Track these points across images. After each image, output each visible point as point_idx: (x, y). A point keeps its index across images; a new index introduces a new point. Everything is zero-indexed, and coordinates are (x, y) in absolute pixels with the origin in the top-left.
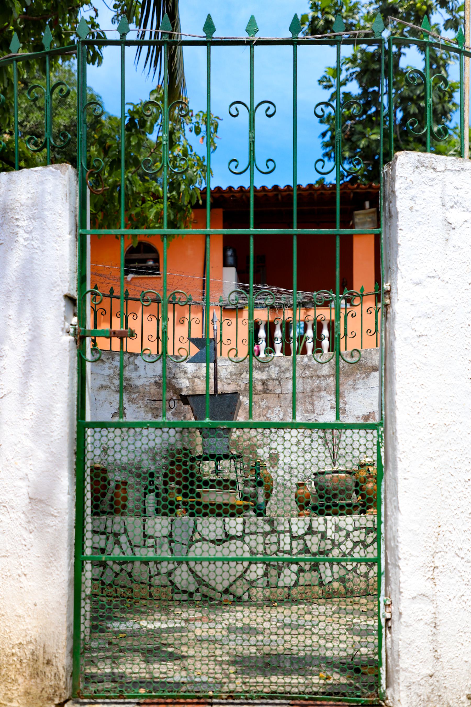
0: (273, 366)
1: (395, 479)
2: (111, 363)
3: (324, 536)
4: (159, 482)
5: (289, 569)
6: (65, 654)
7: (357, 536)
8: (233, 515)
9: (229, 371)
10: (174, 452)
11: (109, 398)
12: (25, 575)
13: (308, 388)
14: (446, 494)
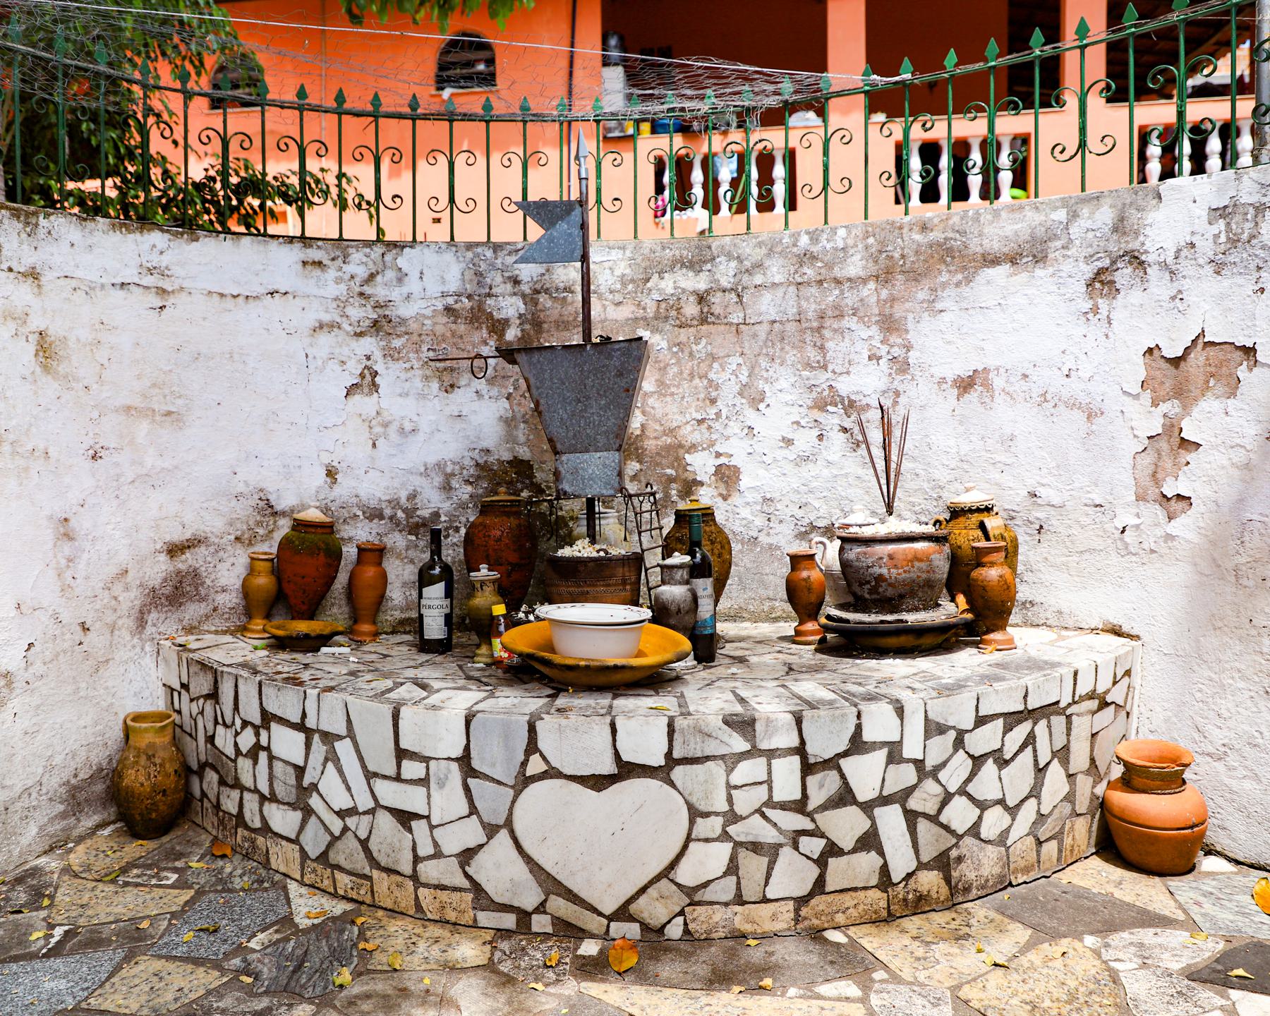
0: (722, 259)
2: (340, 269)
3: (894, 754)
4: (452, 552)
5: (796, 848)
9: (618, 272)
11: (337, 351)
13: (811, 309)
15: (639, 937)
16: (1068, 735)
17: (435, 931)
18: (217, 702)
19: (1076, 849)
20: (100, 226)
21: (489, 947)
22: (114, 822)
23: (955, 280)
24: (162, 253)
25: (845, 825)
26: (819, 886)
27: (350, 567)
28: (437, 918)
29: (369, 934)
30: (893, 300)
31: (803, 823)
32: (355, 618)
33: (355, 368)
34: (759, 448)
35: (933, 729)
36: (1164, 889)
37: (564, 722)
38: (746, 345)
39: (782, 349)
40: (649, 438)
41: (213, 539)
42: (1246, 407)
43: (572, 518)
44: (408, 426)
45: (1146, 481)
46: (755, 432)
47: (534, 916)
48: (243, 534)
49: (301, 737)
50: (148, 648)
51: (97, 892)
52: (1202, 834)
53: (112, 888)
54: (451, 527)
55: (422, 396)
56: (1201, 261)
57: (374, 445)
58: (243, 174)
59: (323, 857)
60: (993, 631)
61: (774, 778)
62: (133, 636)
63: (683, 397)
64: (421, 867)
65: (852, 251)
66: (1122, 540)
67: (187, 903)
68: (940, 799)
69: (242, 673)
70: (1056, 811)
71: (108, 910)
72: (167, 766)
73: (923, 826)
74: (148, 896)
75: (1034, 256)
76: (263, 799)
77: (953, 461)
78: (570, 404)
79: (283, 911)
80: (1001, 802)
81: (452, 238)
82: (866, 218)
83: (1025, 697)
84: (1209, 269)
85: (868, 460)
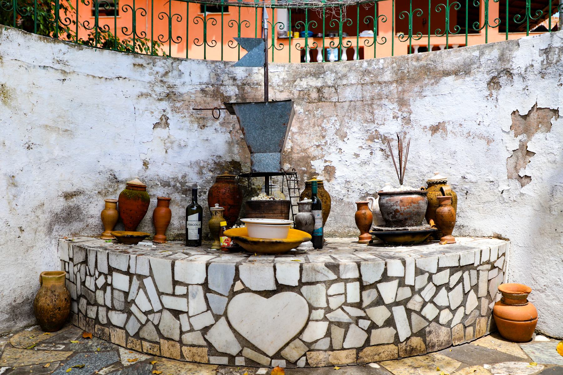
0: (329, 72)
3: (402, 282)
5: (357, 325)
9: (281, 77)
11: (149, 107)
13: (368, 95)
15: (285, 367)
16: (478, 279)
17: (190, 366)
18: (87, 265)
19: (481, 332)
20: (33, 37)
21: (215, 372)
22: (33, 325)
23: (431, 82)
24: (64, 54)
25: (380, 315)
26: (367, 342)
27: (154, 209)
28: (191, 360)
29: (157, 368)
30: (404, 91)
31: (360, 313)
32: (156, 232)
33: (158, 115)
34: (344, 158)
35: (419, 272)
36: (519, 348)
37: (252, 265)
38: (339, 111)
39: (355, 113)
40: (294, 153)
41: (87, 192)
42: (554, 136)
43: (259, 189)
44: (183, 144)
45: (512, 170)
46: (342, 151)
47: (237, 358)
48: (102, 190)
49: (127, 278)
50: (53, 242)
51: (24, 353)
52: (535, 324)
53: (31, 351)
54: (202, 192)
55: (190, 130)
56: (536, 73)
57: (166, 152)
58: (107, 38)
59: (137, 335)
60: (446, 235)
61: (347, 292)
62: (46, 235)
63: (310, 135)
64: (184, 336)
65: (386, 70)
66: (502, 196)
67: (68, 357)
68: (422, 304)
69: (99, 250)
70: (472, 313)
71: (29, 360)
72: (61, 296)
73: (414, 316)
74: (49, 355)
75: (465, 72)
76: (108, 309)
77: (428, 162)
78: (258, 130)
79: (116, 359)
80: (448, 307)
81: (205, 58)
82: (392, 55)
83: (459, 260)
84: (539, 76)
85: (392, 163)
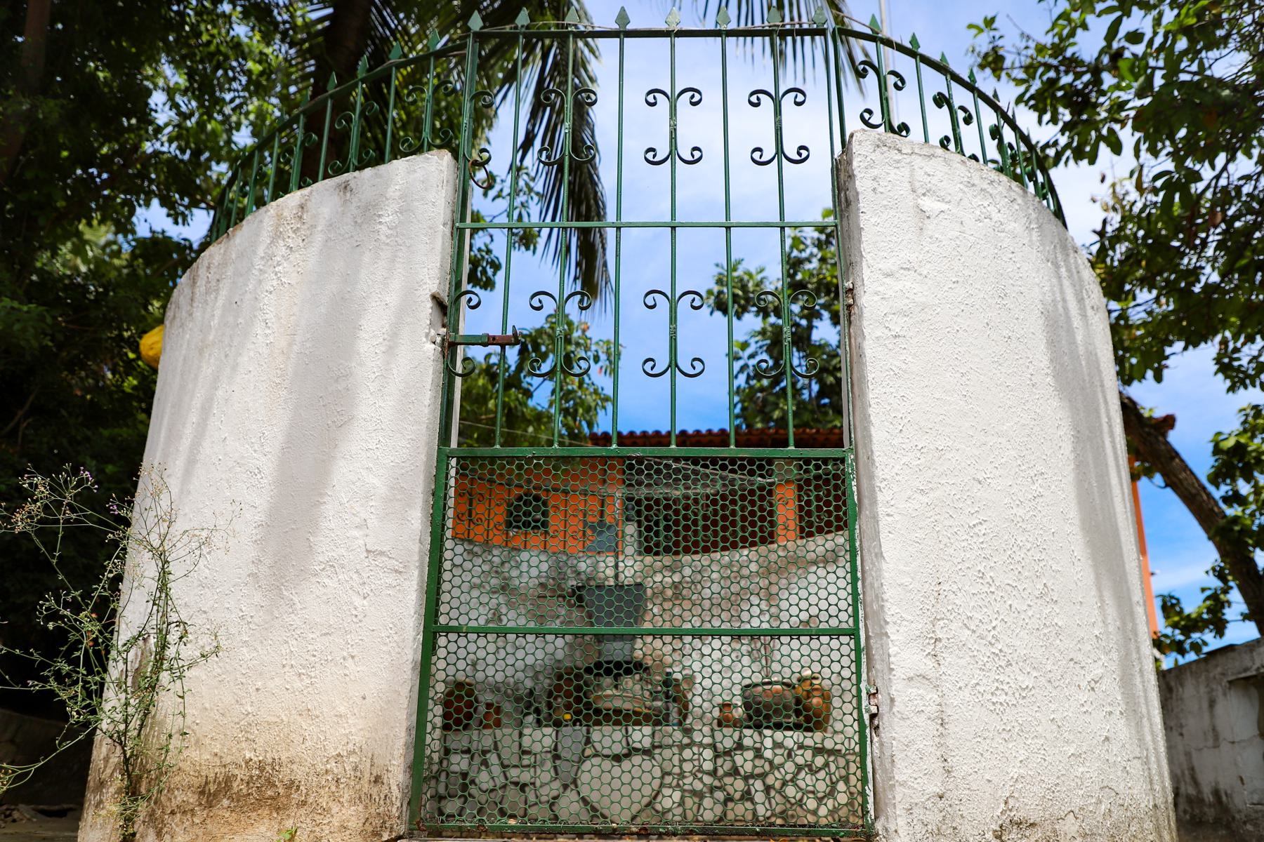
1: (875, 518)
6: (402, 768)
7: (802, 757)
8: (637, 723)
10: (562, 671)
12: (353, 657)
14: (945, 540)
